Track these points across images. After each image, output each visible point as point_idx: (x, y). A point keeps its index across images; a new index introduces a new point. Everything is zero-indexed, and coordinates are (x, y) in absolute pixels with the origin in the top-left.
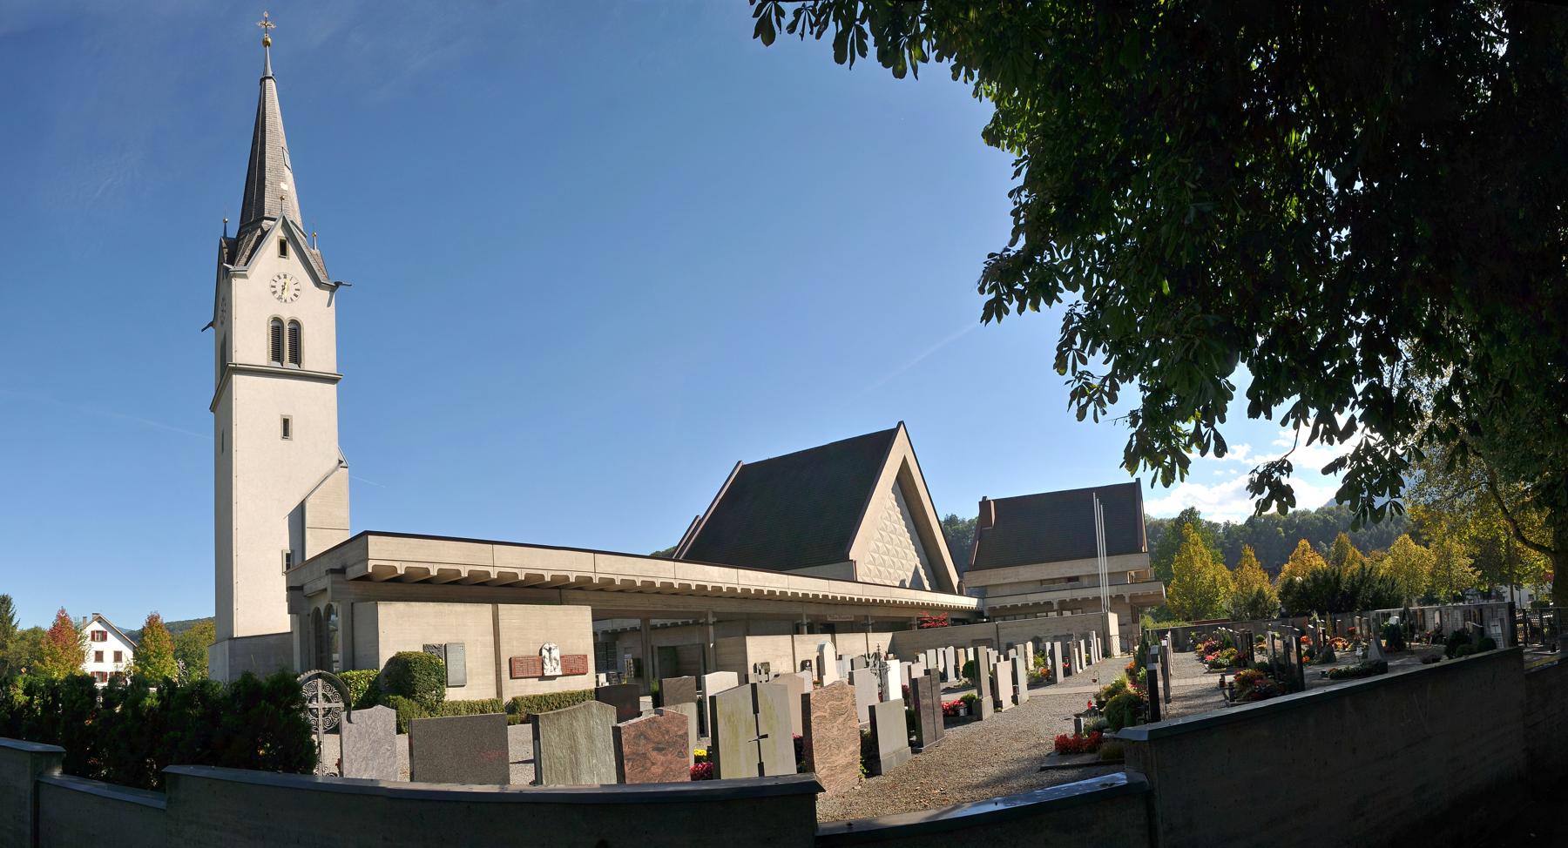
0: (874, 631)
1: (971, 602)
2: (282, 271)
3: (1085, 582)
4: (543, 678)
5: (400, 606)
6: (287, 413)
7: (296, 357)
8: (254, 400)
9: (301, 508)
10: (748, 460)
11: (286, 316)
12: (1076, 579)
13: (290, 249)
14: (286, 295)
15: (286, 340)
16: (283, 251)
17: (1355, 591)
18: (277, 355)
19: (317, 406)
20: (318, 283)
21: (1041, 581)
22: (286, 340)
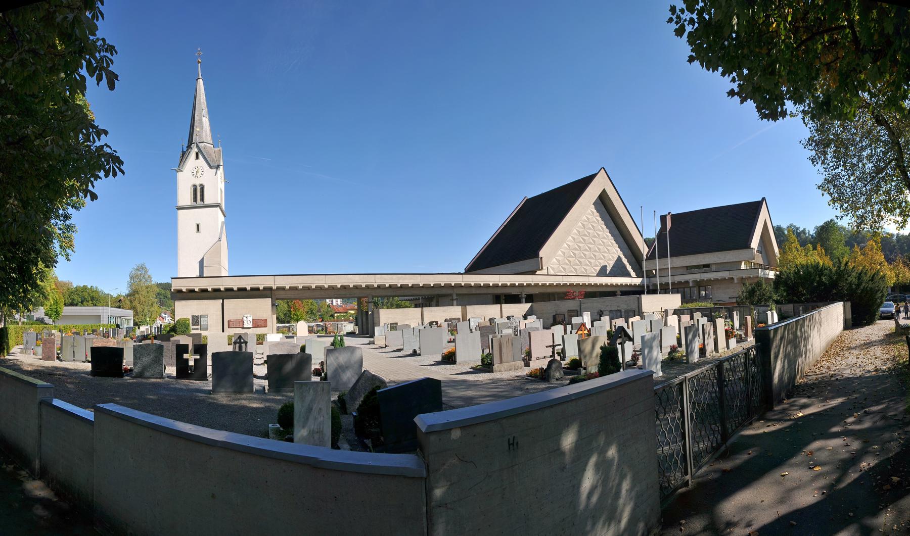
0: (506, 303)
1: (637, 281)
2: (195, 166)
3: (713, 268)
4: (243, 328)
5: (183, 302)
6: (198, 222)
7: (202, 199)
8: (186, 219)
9: (203, 259)
10: (529, 197)
11: (198, 183)
12: (707, 266)
13: (200, 156)
14: (199, 174)
15: (198, 193)
16: (197, 157)
17: (834, 284)
18: (195, 200)
19: (213, 220)
20: (211, 167)
21: (687, 267)
22: (198, 193)
